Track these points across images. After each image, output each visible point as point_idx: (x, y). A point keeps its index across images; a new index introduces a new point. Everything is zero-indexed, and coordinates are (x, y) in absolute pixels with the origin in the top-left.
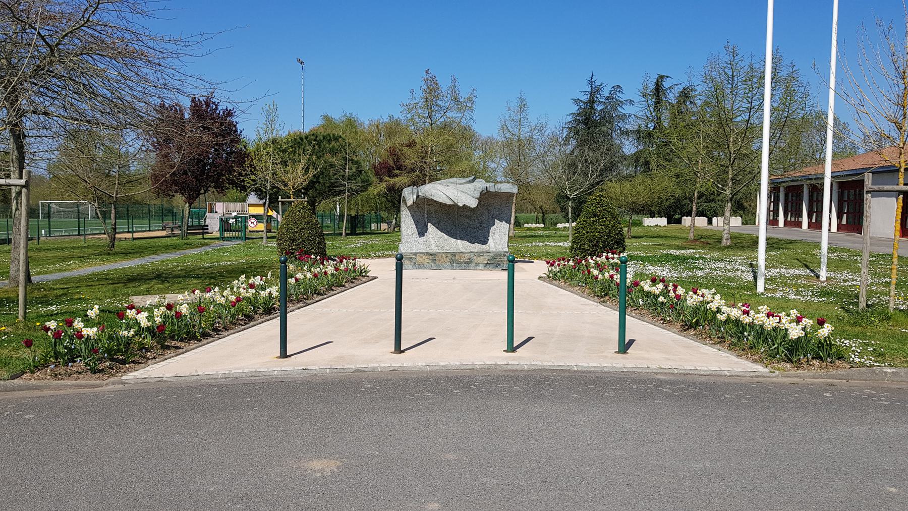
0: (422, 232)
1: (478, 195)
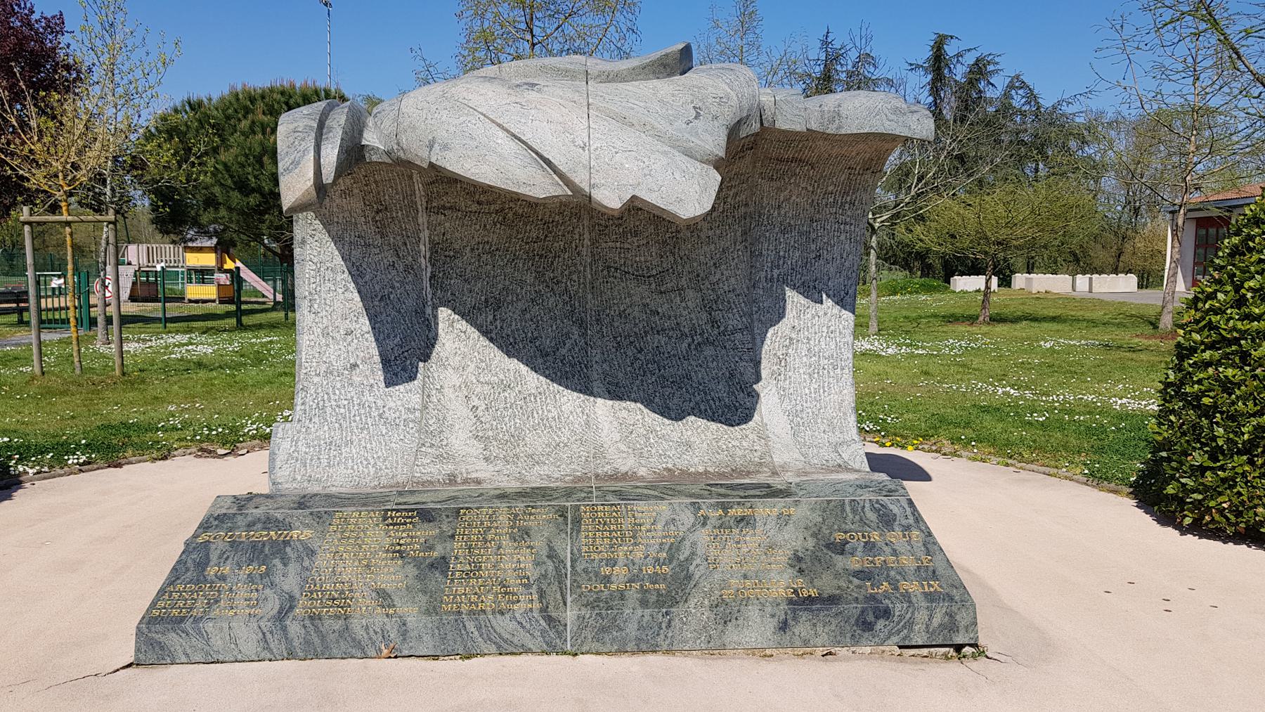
0: (404, 354)
1: (716, 143)
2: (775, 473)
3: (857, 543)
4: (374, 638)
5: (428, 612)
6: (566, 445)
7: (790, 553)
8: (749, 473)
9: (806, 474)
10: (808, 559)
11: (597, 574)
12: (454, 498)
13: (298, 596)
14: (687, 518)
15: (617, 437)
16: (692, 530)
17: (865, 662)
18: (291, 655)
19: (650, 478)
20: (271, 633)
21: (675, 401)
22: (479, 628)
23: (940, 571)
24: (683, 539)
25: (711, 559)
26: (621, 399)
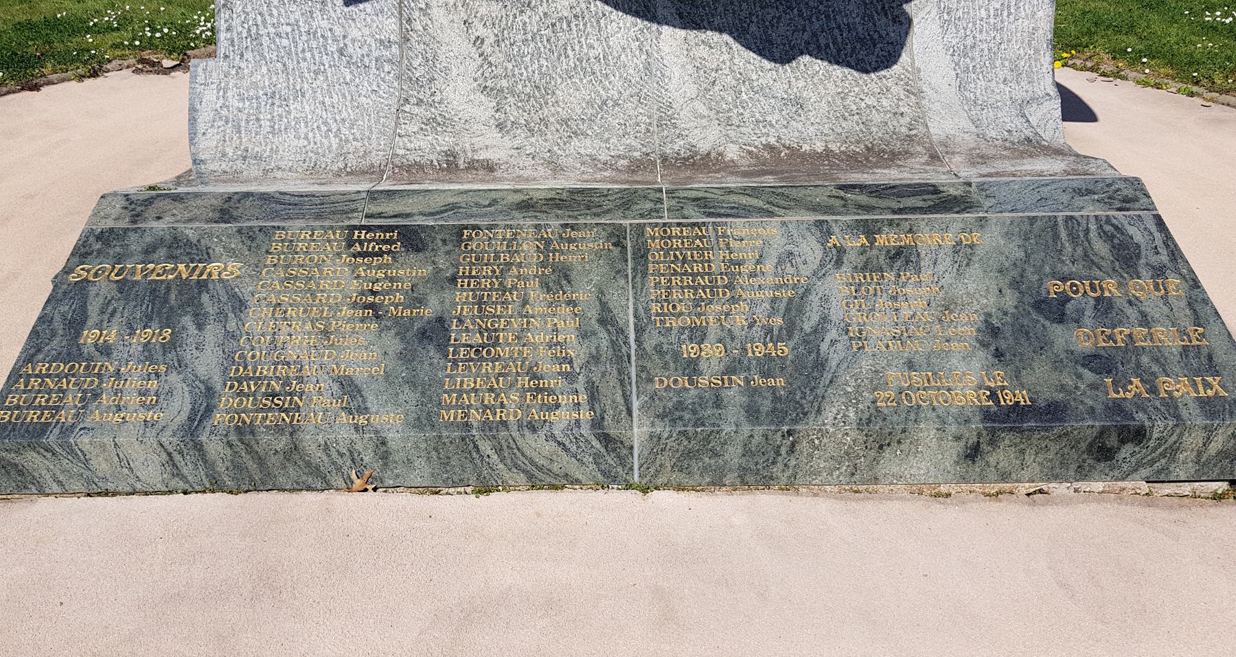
2: (934, 157)
3: (1082, 298)
4: (340, 461)
5: (418, 424)
6: (616, 104)
7: (978, 319)
8: (894, 156)
9: (984, 159)
10: (1008, 331)
11: (677, 356)
12: (453, 207)
13: (218, 387)
14: (811, 251)
15: (692, 90)
16: (819, 274)
17: (1093, 506)
18: (215, 486)
19: (745, 163)
20: (181, 452)
21: (782, 29)
22: (499, 450)
23: (1220, 357)
24: (808, 291)
25: (854, 329)
26: (698, 26)
